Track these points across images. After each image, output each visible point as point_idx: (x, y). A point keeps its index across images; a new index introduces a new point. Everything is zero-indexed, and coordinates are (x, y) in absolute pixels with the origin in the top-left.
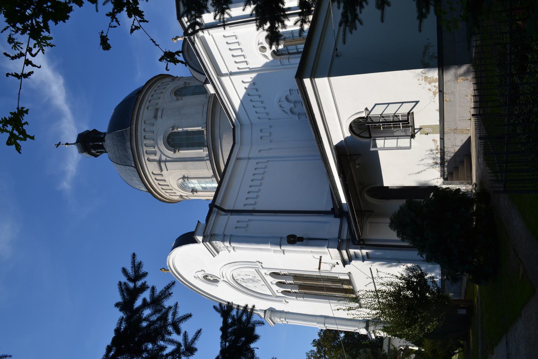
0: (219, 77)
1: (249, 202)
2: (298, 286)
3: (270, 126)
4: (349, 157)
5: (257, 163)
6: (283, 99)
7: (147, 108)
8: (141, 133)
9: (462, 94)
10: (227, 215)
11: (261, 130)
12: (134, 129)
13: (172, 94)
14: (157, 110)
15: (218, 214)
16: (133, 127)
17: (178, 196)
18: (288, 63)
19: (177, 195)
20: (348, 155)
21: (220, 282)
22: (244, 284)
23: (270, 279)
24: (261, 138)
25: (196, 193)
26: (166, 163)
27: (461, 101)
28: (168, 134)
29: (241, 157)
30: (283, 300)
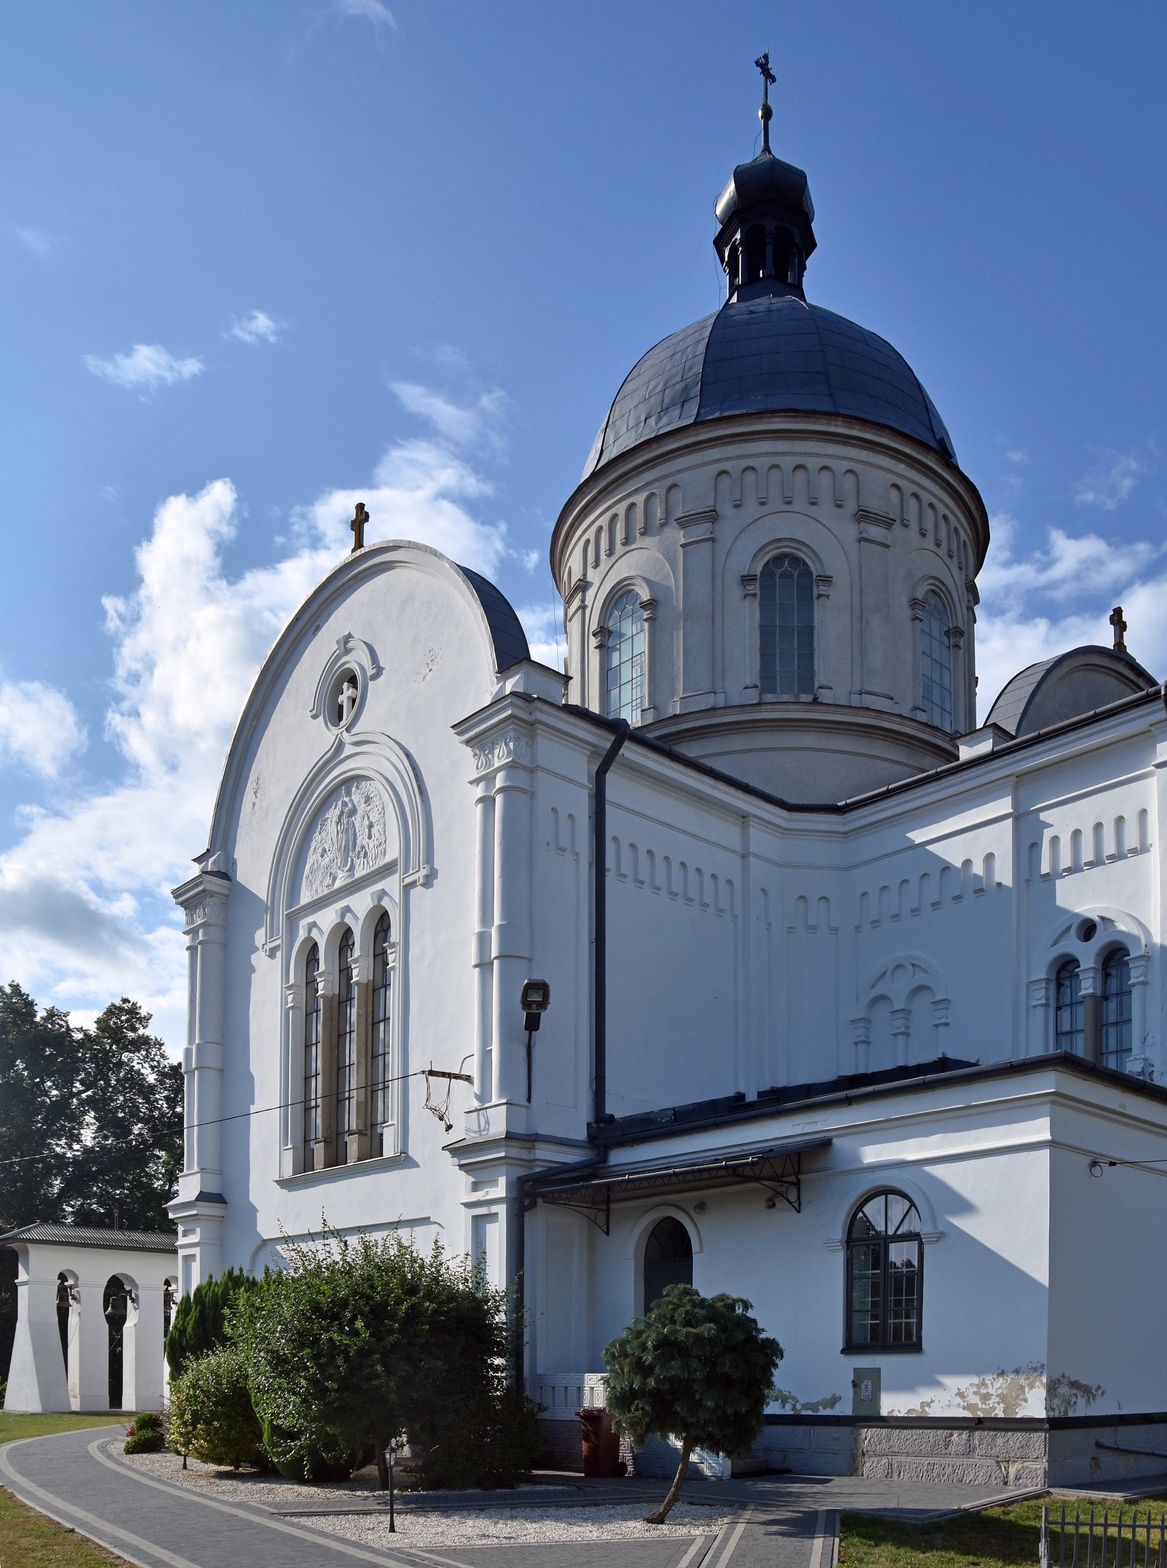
0: (1014, 778)
1: (626, 852)
2: (337, 993)
3: (836, 929)
4: (793, 1179)
5: (729, 882)
6: (920, 979)
7: (895, 486)
8: (816, 455)
9: (966, 1472)
10: (590, 781)
11: (825, 898)
12: (833, 429)
13: (931, 581)
14: (888, 523)
15: (594, 749)
16: (837, 426)
17: (585, 575)
18: (1032, 1004)
19: (590, 570)
20: (800, 1177)
21: (336, 730)
22: (333, 814)
23: (361, 903)
24: (802, 897)
25: (596, 645)
26: (709, 544)
27: (947, 1467)
28: (808, 561)
29: (752, 830)
30: (279, 942)
